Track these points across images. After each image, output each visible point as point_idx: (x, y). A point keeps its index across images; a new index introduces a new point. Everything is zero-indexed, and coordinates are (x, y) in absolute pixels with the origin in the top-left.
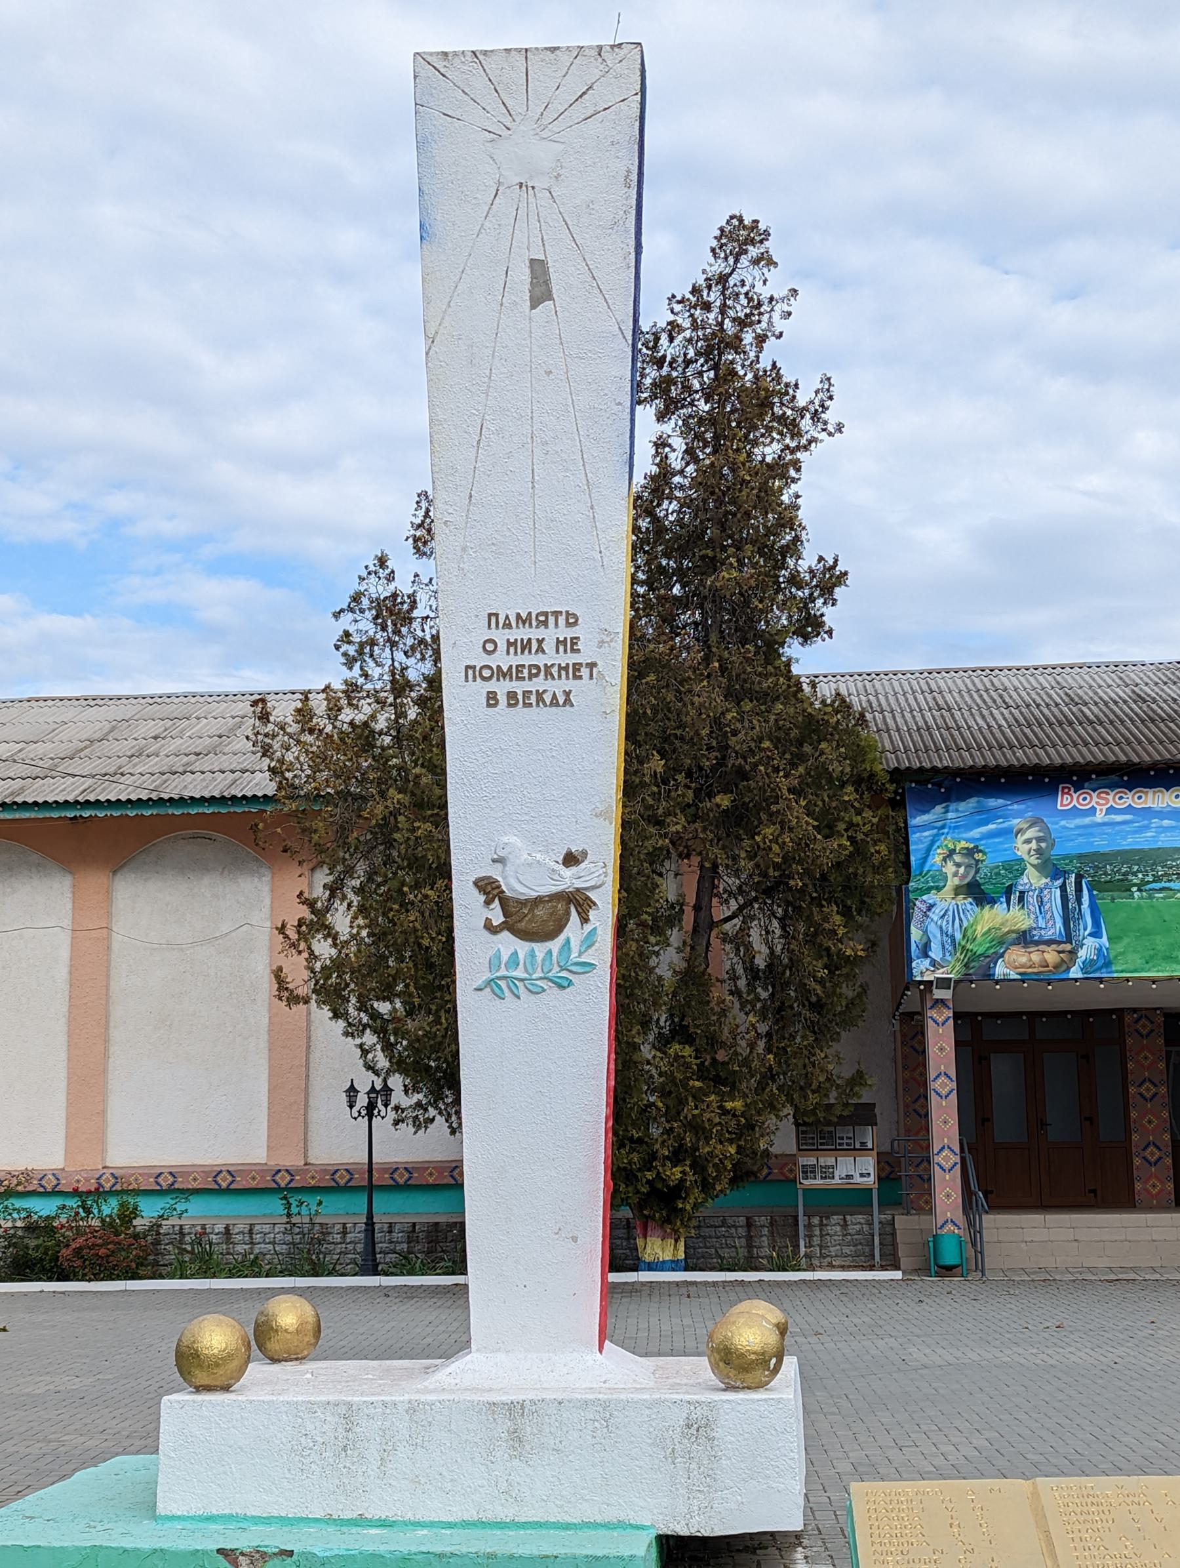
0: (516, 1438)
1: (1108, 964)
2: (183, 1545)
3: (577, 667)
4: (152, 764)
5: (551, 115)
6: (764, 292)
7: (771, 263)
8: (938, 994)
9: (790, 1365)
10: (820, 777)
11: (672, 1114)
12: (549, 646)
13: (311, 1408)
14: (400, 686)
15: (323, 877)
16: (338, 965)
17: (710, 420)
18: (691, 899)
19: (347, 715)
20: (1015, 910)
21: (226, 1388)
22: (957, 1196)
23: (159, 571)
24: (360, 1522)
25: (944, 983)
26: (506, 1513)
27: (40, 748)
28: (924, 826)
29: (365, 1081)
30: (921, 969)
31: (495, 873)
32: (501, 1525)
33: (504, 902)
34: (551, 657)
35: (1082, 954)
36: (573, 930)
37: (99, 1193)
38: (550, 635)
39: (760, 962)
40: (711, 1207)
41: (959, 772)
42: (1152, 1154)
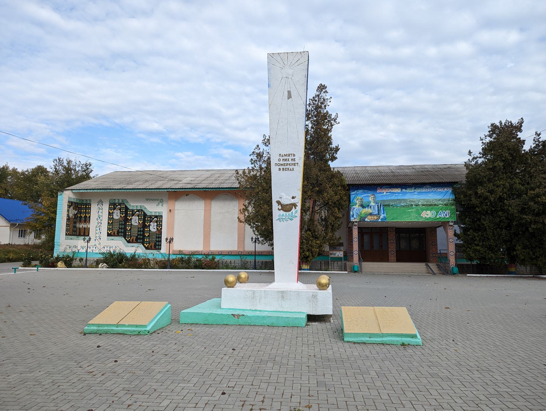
0: (283, 297)
1: (386, 219)
2: (226, 313)
3: (295, 164)
4: (218, 182)
5: (292, 64)
6: (326, 98)
7: (327, 92)
8: (355, 224)
9: (330, 286)
10: (334, 185)
11: (307, 243)
12: (290, 160)
13: (247, 291)
14: (261, 168)
15: (247, 202)
16: (248, 216)
17: (317, 121)
18: (311, 206)
19: (252, 173)
20: (369, 209)
21: (233, 287)
22: (357, 259)
23: (216, 148)
24: (256, 310)
25: (356, 222)
26: (280, 310)
27: (199, 179)
28: (353, 194)
29: (254, 237)
30: (352, 219)
31: (280, 200)
32: (280, 312)
33: (281, 205)
34: (290, 162)
35: (381, 217)
36: (293, 210)
37: (208, 255)
38: (290, 158)
39: (323, 218)
40: (314, 260)
41: (360, 185)
42: (392, 252)
